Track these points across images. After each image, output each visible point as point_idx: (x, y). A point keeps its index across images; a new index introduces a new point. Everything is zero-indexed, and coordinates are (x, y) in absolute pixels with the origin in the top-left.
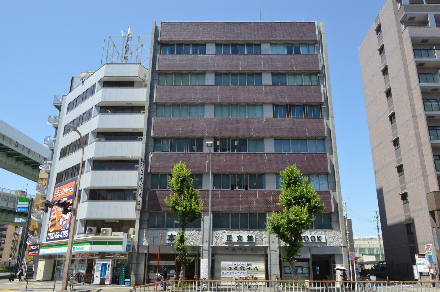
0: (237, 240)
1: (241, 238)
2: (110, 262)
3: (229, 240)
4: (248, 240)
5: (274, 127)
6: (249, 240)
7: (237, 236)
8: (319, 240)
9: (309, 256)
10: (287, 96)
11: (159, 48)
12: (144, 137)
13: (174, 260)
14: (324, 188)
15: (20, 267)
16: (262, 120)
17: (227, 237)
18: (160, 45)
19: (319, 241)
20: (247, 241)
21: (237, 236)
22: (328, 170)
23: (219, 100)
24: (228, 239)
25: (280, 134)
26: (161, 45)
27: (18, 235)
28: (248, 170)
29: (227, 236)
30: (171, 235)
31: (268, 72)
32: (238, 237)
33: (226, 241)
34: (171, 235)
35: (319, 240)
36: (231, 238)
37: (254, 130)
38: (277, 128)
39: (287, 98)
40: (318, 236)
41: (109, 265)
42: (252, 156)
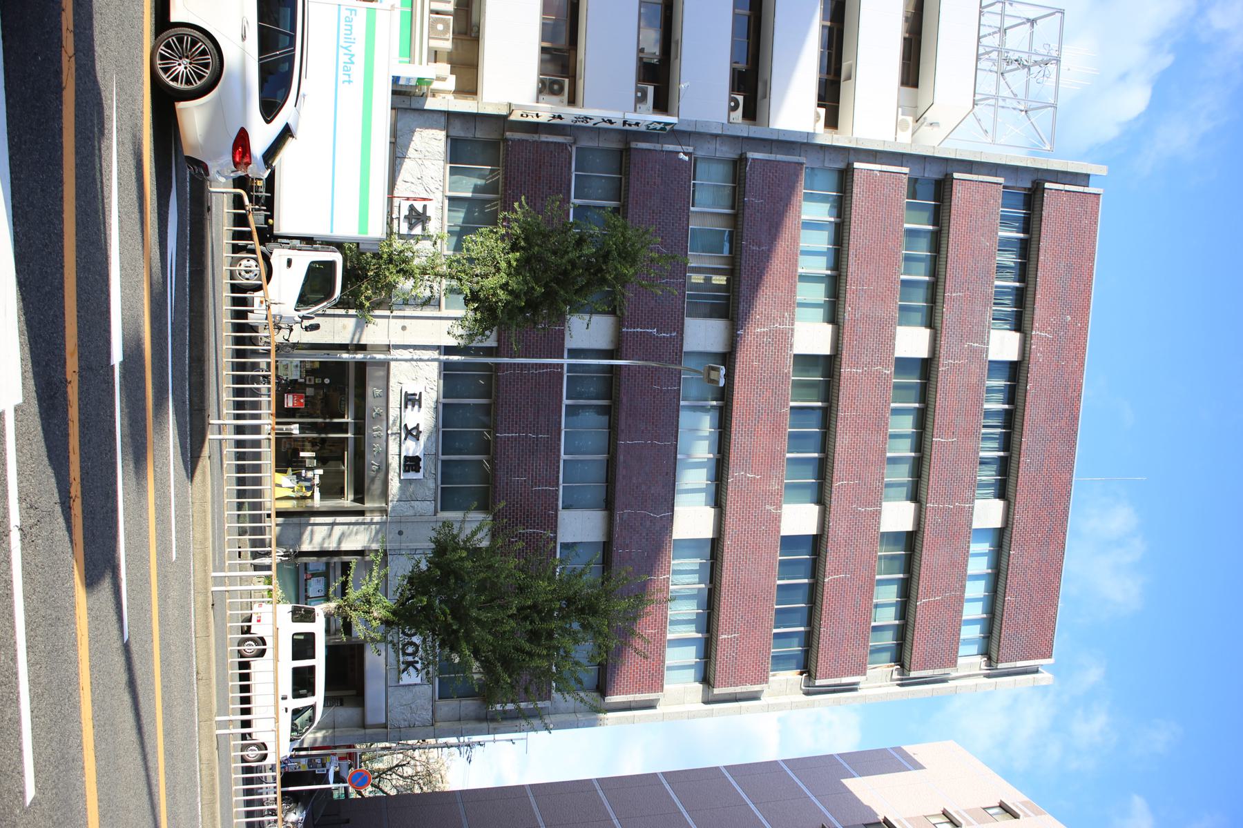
0: (406, 425)
7: (418, 425)
19: (402, 667)
23: (846, 370)
24: (409, 397)
32: (417, 427)
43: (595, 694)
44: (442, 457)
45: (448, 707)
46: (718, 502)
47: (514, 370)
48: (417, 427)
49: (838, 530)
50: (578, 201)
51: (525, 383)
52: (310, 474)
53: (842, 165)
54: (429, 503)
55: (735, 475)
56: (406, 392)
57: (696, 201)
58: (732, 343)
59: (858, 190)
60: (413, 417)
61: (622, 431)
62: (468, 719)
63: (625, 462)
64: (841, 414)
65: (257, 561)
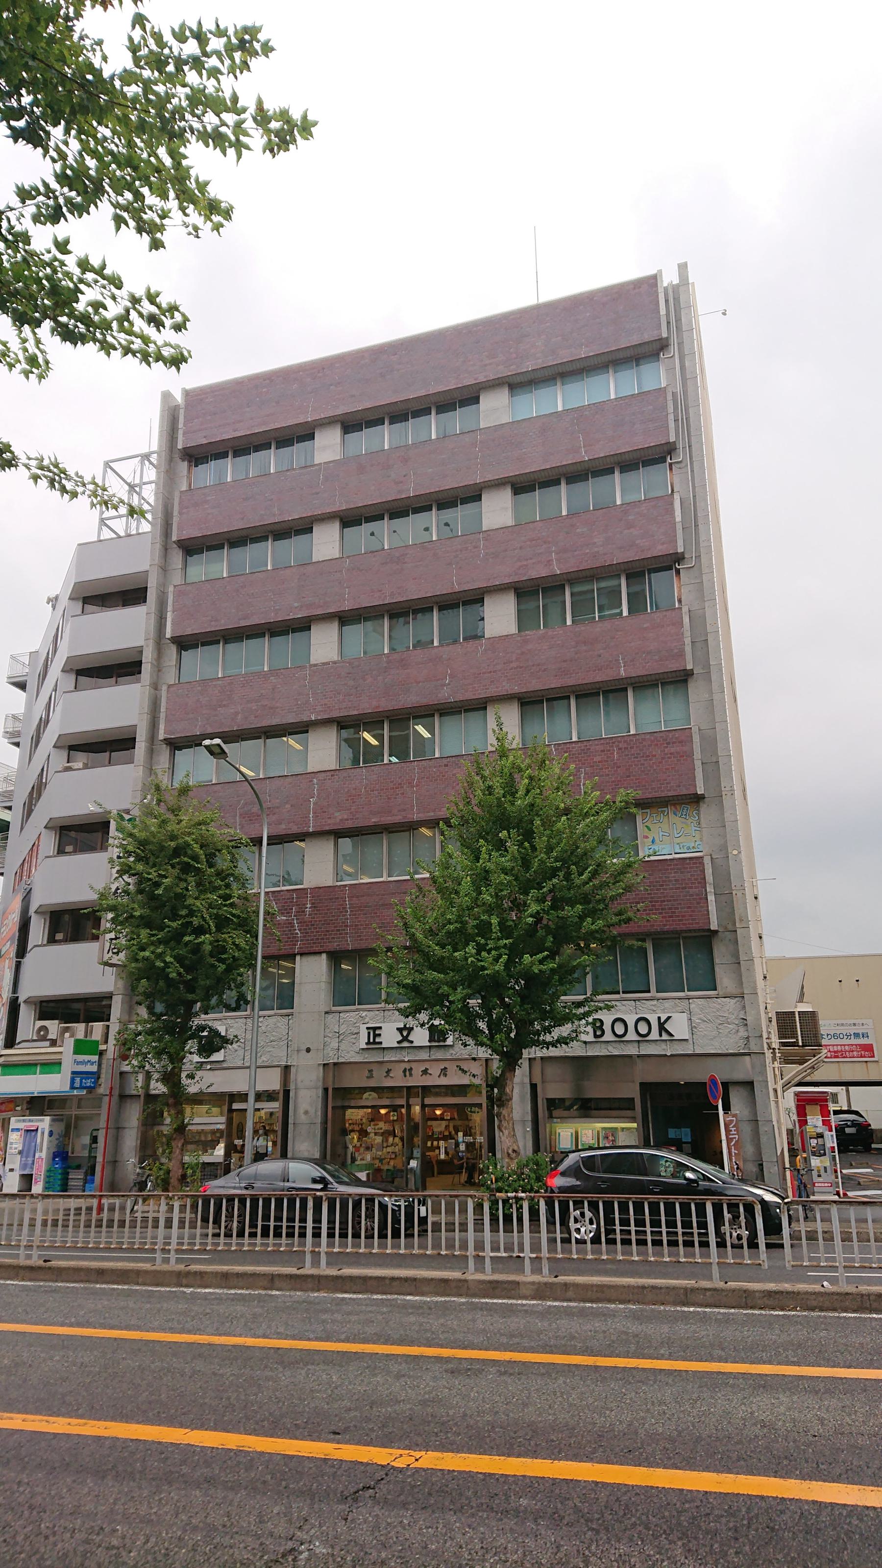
0: (399, 1042)
1: (408, 1034)
2: (44, 1123)
3: (375, 1043)
4: (430, 1041)
5: (512, 665)
6: (435, 1041)
7: (398, 1029)
8: (663, 1033)
9: (633, 1091)
10: (557, 554)
11: (185, 472)
12: (141, 746)
13: (482, 920)
14: (689, 848)
15: (384, 1107)
16: (477, 647)
17: (369, 1033)
18: (186, 463)
19: (665, 1037)
20: (428, 1044)
21: (398, 1029)
22: (695, 786)
23: (347, 606)
24: (371, 1040)
25: (534, 685)
26: (190, 462)
27: (275, 1132)
28: (432, 814)
29: (368, 1028)
30: (194, 71)
31: (498, 484)
32: (400, 1030)
33: (365, 1046)
34: (194, 71)
35: (663, 1033)
36: (380, 1035)
37: (450, 681)
38: (521, 667)
39: (557, 560)
40: (659, 1018)
41: (43, 1133)
42: (446, 765)
43: (701, 804)
44: (653, 993)
45: (725, 980)
46: (480, 706)
47: (347, 933)
48: (400, 1030)
49: (505, 573)
50: (385, 874)
51: (359, 921)
52: (462, 1147)
53: (173, 649)
54: (692, 1006)
55: (446, 694)
56: (367, 1044)
57: (209, 779)
58: (509, 698)
59: (190, 629)
60: (390, 1037)
61: (405, 817)
62: (736, 955)
63: (434, 811)
64: (457, 588)
65: (310, 1204)
